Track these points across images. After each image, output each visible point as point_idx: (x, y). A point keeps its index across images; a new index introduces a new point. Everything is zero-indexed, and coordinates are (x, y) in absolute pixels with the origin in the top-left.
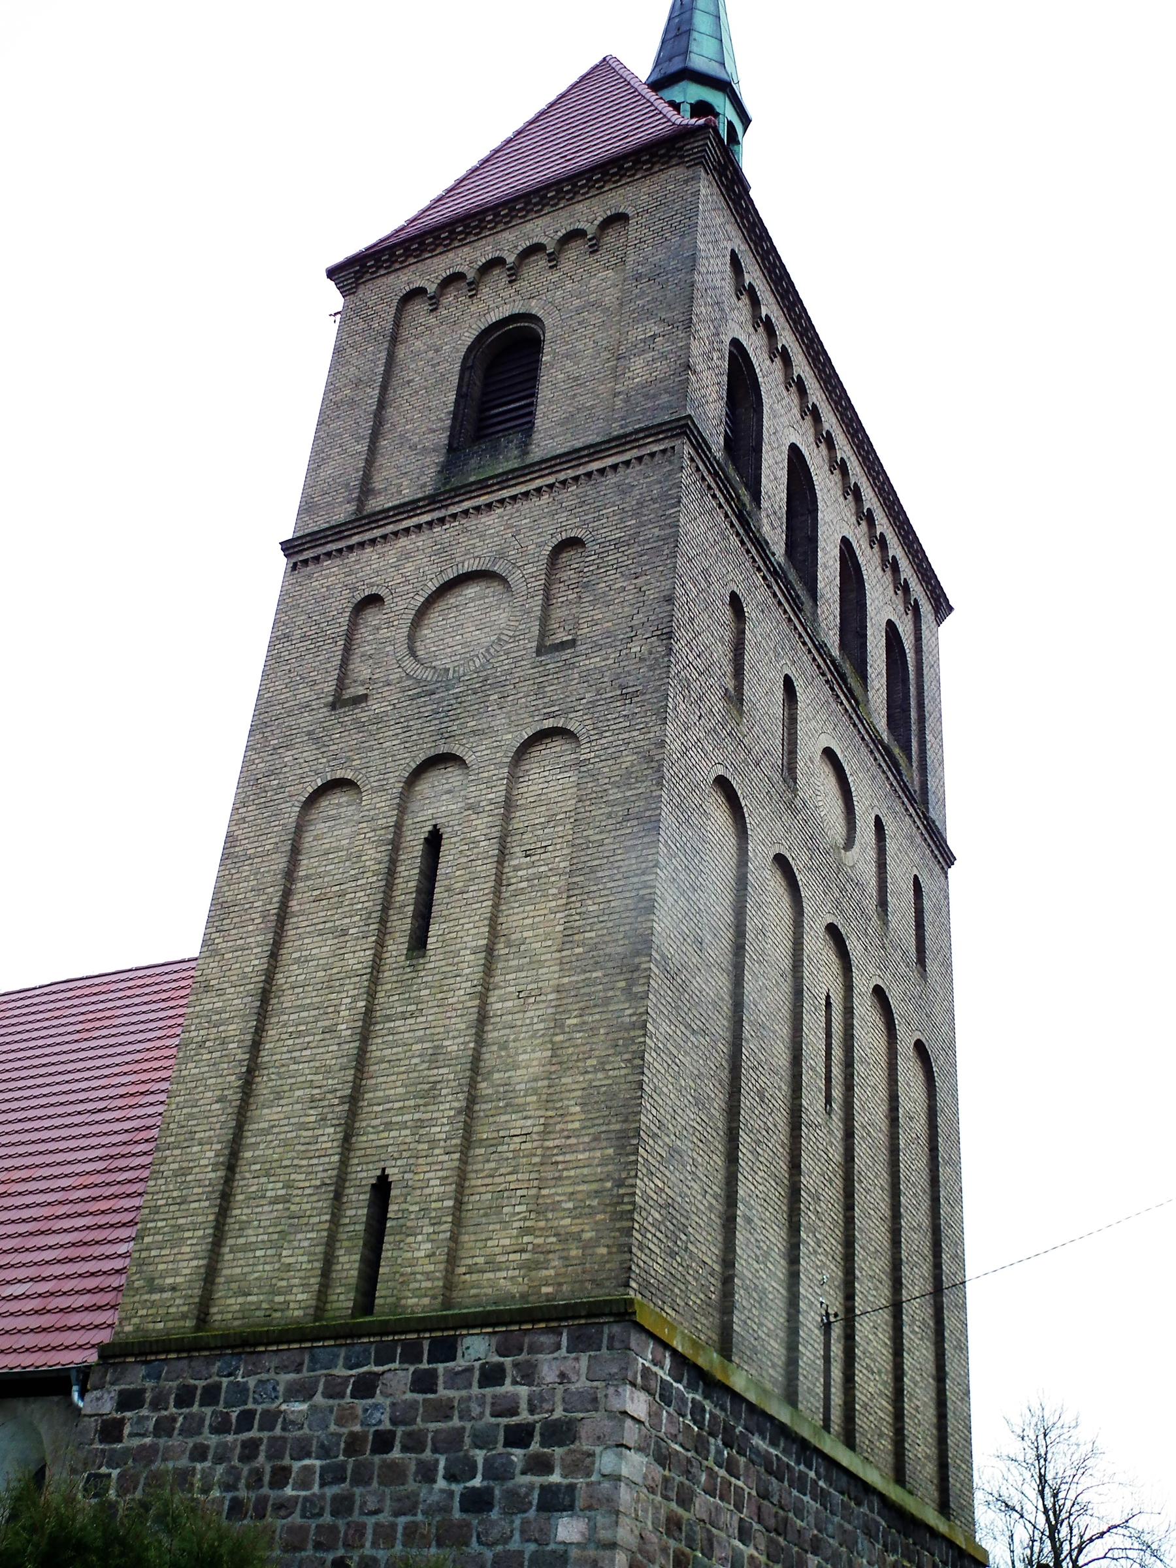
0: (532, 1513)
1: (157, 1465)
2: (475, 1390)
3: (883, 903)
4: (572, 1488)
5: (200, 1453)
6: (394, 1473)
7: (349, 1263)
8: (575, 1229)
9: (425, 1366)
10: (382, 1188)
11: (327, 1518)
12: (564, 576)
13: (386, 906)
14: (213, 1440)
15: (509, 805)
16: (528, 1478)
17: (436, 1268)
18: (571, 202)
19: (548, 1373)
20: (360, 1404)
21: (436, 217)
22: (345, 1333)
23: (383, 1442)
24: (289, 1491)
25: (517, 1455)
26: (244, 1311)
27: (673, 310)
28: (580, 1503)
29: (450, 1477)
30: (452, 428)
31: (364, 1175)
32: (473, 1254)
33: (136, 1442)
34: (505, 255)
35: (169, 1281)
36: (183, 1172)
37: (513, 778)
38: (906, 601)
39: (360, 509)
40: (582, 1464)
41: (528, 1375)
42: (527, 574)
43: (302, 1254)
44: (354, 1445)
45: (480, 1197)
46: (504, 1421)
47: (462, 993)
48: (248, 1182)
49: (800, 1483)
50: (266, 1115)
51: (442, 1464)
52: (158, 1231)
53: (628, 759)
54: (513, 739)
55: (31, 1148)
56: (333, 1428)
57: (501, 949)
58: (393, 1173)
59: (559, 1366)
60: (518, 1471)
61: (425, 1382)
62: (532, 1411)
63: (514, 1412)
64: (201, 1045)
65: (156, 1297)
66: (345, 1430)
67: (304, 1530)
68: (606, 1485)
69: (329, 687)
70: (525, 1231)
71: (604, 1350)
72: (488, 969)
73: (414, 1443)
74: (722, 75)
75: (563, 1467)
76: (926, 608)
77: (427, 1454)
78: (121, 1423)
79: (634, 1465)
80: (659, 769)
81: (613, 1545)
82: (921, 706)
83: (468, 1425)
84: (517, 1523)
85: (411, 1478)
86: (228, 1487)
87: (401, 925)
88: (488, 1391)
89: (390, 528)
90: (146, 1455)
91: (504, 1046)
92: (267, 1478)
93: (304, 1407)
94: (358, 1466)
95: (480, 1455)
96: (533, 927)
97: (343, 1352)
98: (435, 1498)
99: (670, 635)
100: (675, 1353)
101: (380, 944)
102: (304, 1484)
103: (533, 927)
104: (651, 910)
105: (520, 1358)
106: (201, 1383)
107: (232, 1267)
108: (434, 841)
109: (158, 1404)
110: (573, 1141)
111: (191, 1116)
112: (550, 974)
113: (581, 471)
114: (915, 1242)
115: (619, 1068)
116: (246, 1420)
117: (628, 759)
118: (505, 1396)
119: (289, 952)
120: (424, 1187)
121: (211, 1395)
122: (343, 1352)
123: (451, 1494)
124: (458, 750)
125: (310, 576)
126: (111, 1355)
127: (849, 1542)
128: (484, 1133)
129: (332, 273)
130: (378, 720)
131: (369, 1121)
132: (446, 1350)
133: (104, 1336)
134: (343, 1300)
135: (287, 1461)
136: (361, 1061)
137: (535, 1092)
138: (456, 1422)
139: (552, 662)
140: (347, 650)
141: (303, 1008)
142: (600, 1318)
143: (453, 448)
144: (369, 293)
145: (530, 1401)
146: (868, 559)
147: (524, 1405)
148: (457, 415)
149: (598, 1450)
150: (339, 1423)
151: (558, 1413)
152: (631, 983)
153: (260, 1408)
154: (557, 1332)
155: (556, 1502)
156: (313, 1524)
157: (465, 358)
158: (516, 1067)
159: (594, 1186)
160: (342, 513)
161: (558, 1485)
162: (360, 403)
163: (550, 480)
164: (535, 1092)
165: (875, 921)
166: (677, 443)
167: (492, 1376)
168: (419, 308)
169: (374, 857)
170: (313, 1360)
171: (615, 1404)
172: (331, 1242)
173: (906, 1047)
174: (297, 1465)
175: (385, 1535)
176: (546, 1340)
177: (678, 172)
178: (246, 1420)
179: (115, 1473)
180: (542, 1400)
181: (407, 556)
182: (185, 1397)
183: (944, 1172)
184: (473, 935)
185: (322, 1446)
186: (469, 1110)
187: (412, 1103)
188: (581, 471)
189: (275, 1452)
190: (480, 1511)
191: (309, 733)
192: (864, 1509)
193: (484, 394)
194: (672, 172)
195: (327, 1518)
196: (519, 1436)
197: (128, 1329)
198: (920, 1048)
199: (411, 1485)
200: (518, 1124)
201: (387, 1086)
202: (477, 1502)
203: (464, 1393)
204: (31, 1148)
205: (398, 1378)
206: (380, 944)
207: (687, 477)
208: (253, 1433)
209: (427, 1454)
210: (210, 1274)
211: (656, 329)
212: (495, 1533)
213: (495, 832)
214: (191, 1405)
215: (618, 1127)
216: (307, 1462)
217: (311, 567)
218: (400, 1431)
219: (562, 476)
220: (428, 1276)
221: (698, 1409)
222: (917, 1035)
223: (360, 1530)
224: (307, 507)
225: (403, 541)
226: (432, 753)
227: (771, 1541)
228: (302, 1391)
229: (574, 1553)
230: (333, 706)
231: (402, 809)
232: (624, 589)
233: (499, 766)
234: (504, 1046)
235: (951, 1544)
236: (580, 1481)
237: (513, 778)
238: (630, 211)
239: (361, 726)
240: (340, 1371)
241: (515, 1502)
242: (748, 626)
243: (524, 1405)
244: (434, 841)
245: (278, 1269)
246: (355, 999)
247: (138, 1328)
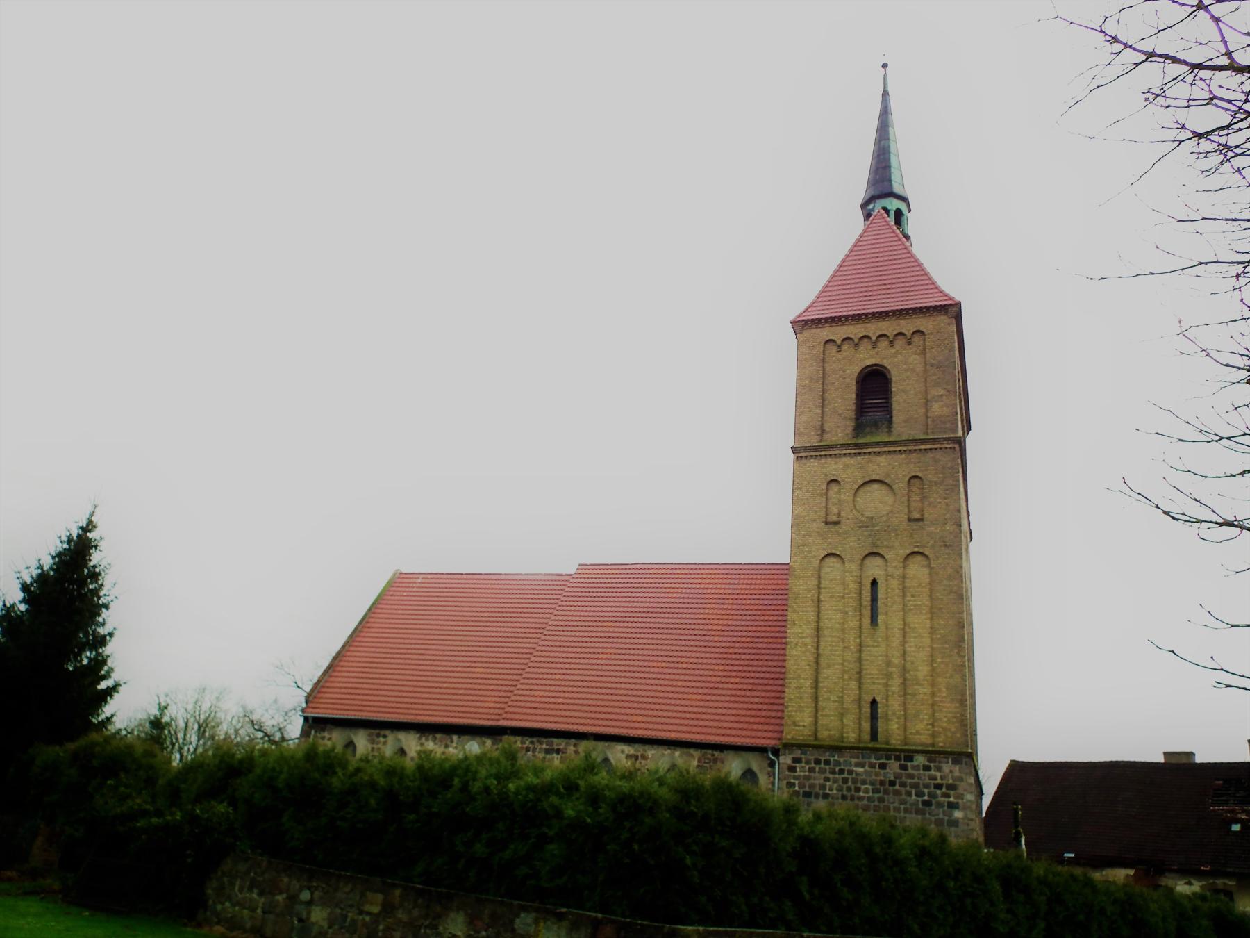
5: (827, 779)
6: (897, 793)
25: (938, 792)
26: (830, 736)
41: (939, 769)
44: (882, 783)
48: (823, 694)
50: (825, 673)
53: (950, 571)
54: (904, 552)
58: (878, 699)
69: (823, 514)
73: (903, 785)
95: (926, 791)
109: (808, 762)
115: (957, 679)
119: (824, 614)
121: (827, 762)
130: (846, 533)
132: (910, 759)
151: (951, 781)
155: (952, 806)
162: (813, 388)
167: (927, 768)
172: (860, 719)
178: (842, 771)
181: (846, 466)
184: (896, 623)
196: (938, 787)
199: (904, 797)
202: (927, 804)
205: (894, 766)
217: (804, 461)
239: (839, 534)
240: (873, 760)
241: (940, 805)
245: (852, 729)
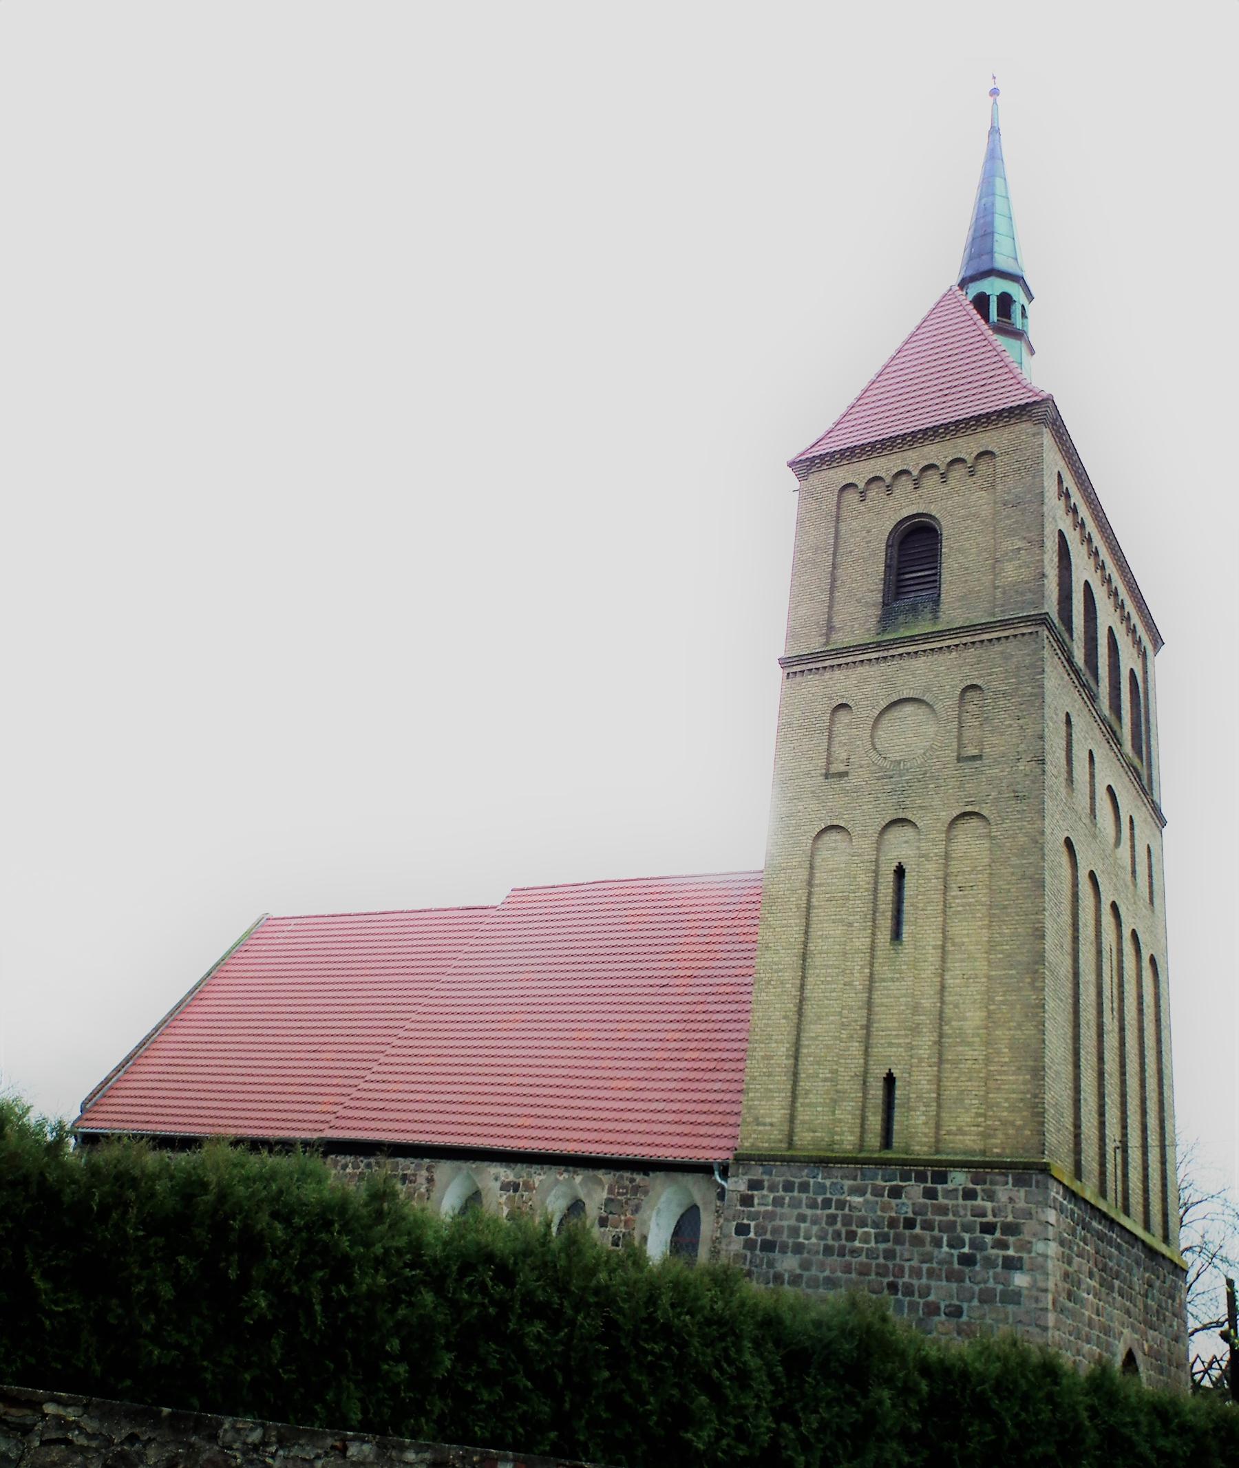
0: (999, 1269)
1: (777, 1223)
2: (961, 1201)
3: (1134, 872)
4: (1020, 1259)
5: (802, 1218)
6: (917, 1241)
7: (875, 1122)
8: (1011, 1119)
9: (929, 1185)
10: (890, 1080)
11: (881, 1260)
12: (970, 708)
14: (809, 1212)
15: (947, 857)
16: (995, 1251)
17: (930, 1130)
18: (954, 437)
20: (894, 1202)
23: (910, 1224)
24: (857, 1244)
25: (988, 1238)
27: (1030, 532)
28: (1026, 1266)
29: (950, 1246)
32: (950, 1125)
33: (762, 1209)
34: (911, 469)
35: (768, 1120)
36: (767, 1058)
37: (948, 840)
38: (1139, 650)
40: (1026, 1246)
41: (990, 1196)
42: (947, 704)
43: (847, 1112)
44: (893, 1223)
45: (950, 1092)
46: (979, 1220)
47: (929, 970)
48: (807, 1067)
49: (1110, 1242)
50: (812, 1029)
51: (945, 1239)
52: (757, 1091)
53: (1022, 839)
56: (879, 1213)
57: (950, 947)
58: (896, 1073)
59: (1008, 1196)
60: (989, 1245)
61: (930, 1194)
62: (994, 1216)
63: (984, 1215)
64: (768, 983)
65: (761, 1128)
66: (887, 1215)
67: (868, 1266)
68: (1040, 1259)
69: (822, 763)
70: (978, 1115)
71: (1034, 1188)
72: (943, 960)
73: (928, 1226)
74: (1018, 272)
75: (1015, 1247)
76: (1147, 642)
77: (936, 1232)
78: (752, 1197)
79: (1053, 1249)
80: (1042, 849)
81: (1046, 1291)
82: (1147, 721)
83: (958, 1220)
84: (991, 1273)
85: (927, 1244)
87: (886, 923)
88: (969, 1203)
90: (770, 1216)
91: (956, 1006)
92: (843, 1236)
93: (861, 1199)
94: (896, 1235)
95: (967, 1236)
96: (968, 935)
97: (880, 1173)
98: (942, 1256)
99: (1043, 762)
100: (1064, 1185)
102: (867, 1241)
103: (968, 935)
104: (1043, 937)
105: (985, 1187)
106: (797, 1181)
107: (803, 1115)
108: (900, 872)
109: (772, 1188)
110: (1005, 1068)
111: (767, 1025)
112: (982, 966)
113: (976, 638)
114: (1151, 1083)
115: (1030, 1030)
116: (827, 1204)
117: (1022, 839)
118: (978, 1206)
119: (815, 931)
120: (916, 1086)
121: (804, 1187)
122: (880, 1173)
123: (952, 1255)
124: (910, 817)
125: (799, 684)
127: (1130, 1270)
128: (949, 1056)
129: (790, 466)
130: (857, 789)
131: (878, 1038)
132: (941, 1178)
134: (874, 1141)
135: (854, 1228)
136: (869, 1004)
137: (978, 1035)
138: (951, 1217)
139: (968, 768)
141: (827, 966)
144: (814, 479)
145: (993, 1211)
146: (1100, 593)
147: (989, 1213)
148: (886, 581)
149: (1034, 1240)
150: (883, 1210)
151: (1010, 1219)
152: (1034, 980)
153: (834, 1198)
155: (1012, 1265)
156: (874, 1262)
158: (965, 1019)
159: (1021, 1096)
161: (1013, 1257)
162: (822, 564)
163: (956, 642)
164: (978, 1035)
165: (1132, 887)
166: (1039, 629)
167: (969, 1195)
168: (851, 497)
169: (864, 879)
170: (862, 1174)
171: (1043, 1218)
173: (1127, 934)
174: (860, 1231)
175: (916, 1273)
179: (753, 1224)
180: (1000, 1210)
181: (864, 680)
182: (788, 1187)
183: (1164, 1034)
184: (932, 938)
185: (874, 1222)
186: (939, 1043)
187: (903, 1032)
188: (976, 638)
189: (847, 1221)
190: (969, 1265)
191: (813, 792)
192: (1135, 1250)
193: (899, 562)
194: (1024, 425)
195: (881, 1260)
196: (988, 1228)
197: (747, 1144)
198: (1153, 960)
199: (928, 1248)
200: (970, 1054)
201: (887, 1022)
202: (967, 1260)
203: (954, 1202)
204: (293, 1055)
205: (914, 1190)
207: (1047, 653)
208: (832, 1211)
209: (936, 1232)
210: (792, 1118)
211: (1020, 544)
212: (979, 1278)
213: (940, 874)
214: (792, 1191)
215: (1032, 1063)
216: (866, 1229)
218: (919, 1219)
219: (964, 640)
220: (926, 1135)
221: (1073, 1212)
222: (1066, 834)
223: (902, 1269)
224: (792, 635)
225: (860, 669)
226: (895, 817)
227: (1101, 1276)
228: (861, 1191)
229: (1025, 1292)
230: (827, 776)
232: (1011, 726)
233: (940, 832)
234: (956, 1006)
235: (1171, 1261)
236: (1025, 1255)
237: (948, 840)
238: (995, 450)
239: (846, 793)
240: (880, 1183)
241: (989, 1263)
242: (1074, 729)
243: (989, 1213)
244: (900, 872)
246: (862, 967)
247: (753, 1145)
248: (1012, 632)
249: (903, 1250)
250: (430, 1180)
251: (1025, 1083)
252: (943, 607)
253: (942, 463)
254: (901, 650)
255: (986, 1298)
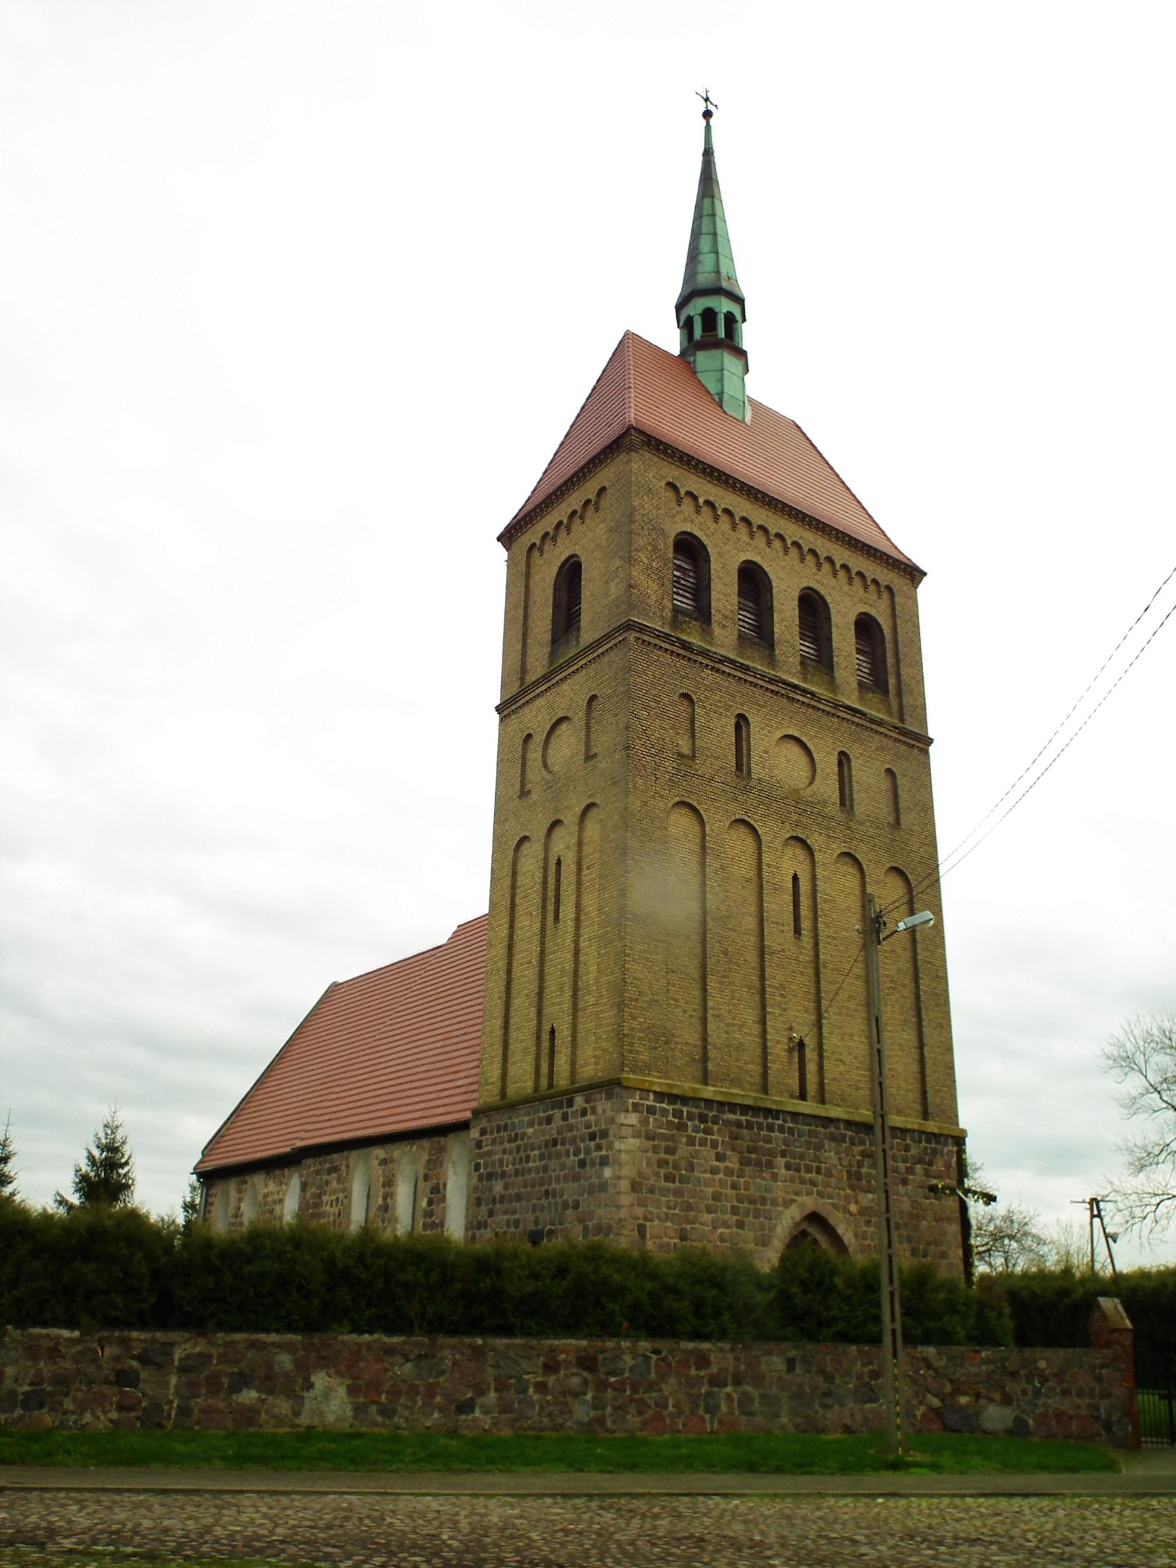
5: (504, 1152)
6: (558, 1155)
13: (544, 900)
19: (599, 1110)
21: (540, 497)
22: (541, 1099)
23: (555, 1143)
24: (531, 1164)
30: (552, 630)
31: (546, 1028)
39: (522, 684)
40: (610, 1147)
54: (578, 810)
55: (399, 1061)
59: (603, 1106)
61: (565, 1117)
69: (518, 787)
86: (514, 1164)
89: (533, 694)
101: (544, 918)
102: (534, 1162)
119: (518, 925)
121: (506, 1127)
126: (476, 1113)
132: (570, 1103)
133: (474, 1105)
134: (544, 1083)
140: (524, 765)
142: (611, 1086)
143: (554, 641)
148: (554, 621)
154: (600, 1092)
155: (604, 1162)
157: (555, 584)
160: (515, 688)
176: (598, 1096)
177: (623, 457)
181: (539, 711)
196: (592, 1137)
204: (399, 1061)
206: (544, 918)
213: (575, 860)
228: (531, 1124)
230: (520, 797)
231: (546, 849)
248: (613, 642)
249: (552, 1164)
250: (347, 1166)
251: (615, 1016)
252: (582, 632)
253: (593, 497)
254: (582, 663)
255: (591, 1191)
